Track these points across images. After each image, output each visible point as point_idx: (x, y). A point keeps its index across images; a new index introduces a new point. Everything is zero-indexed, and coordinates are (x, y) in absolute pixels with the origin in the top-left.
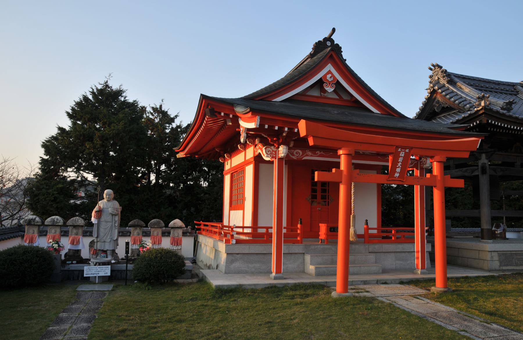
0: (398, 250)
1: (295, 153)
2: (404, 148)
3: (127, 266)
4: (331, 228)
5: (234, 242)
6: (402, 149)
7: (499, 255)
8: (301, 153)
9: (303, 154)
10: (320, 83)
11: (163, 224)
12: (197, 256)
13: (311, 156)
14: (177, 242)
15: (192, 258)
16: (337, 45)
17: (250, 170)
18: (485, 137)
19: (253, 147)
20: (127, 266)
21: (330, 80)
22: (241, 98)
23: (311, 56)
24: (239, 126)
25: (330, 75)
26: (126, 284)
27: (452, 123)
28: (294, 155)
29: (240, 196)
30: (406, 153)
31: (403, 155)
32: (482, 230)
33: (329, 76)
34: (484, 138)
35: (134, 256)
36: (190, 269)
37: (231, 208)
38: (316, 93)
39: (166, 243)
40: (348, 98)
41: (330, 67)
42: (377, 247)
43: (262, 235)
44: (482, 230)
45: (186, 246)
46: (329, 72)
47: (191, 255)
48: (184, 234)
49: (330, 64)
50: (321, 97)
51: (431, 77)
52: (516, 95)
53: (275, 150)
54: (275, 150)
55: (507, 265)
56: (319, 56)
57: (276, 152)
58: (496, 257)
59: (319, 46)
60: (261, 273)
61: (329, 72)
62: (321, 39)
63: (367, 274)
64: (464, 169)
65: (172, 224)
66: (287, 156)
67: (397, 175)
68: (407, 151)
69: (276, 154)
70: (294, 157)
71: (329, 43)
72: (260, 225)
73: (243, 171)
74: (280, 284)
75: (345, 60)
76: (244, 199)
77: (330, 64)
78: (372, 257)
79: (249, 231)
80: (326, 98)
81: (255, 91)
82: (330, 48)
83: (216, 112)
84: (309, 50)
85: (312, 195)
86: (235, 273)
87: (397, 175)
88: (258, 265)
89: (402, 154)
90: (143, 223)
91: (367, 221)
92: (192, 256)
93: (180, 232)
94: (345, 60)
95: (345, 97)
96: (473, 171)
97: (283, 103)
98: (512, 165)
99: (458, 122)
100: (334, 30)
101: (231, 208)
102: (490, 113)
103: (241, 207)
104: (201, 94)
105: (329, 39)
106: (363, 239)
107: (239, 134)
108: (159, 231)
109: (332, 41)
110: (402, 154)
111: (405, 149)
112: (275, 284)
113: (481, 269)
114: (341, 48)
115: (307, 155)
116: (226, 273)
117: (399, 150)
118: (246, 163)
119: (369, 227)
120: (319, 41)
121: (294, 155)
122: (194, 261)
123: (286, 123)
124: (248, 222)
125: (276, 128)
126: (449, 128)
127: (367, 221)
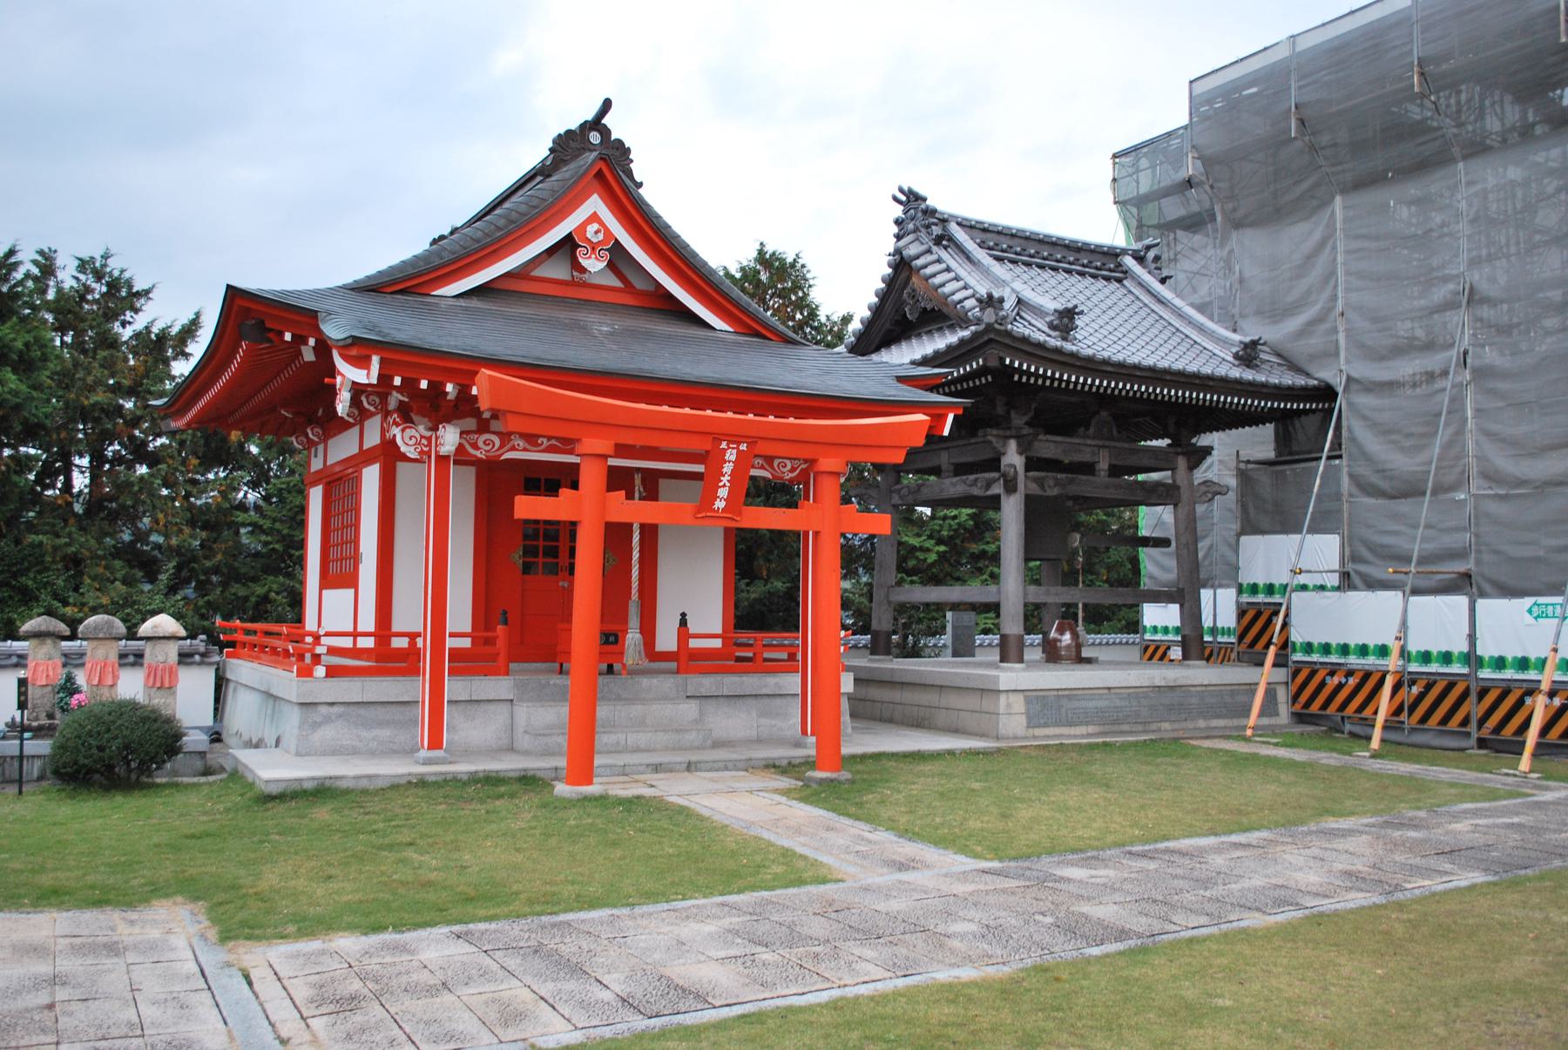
0: (765, 691)
1: (480, 444)
2: (735, 439)
3: (22, 745)
4: (616, 642)
5: (320, 671)
6: (729, 442)
7: (1028, 701)
8: (498, 444)
9: (501, 446)
10: (568, 245)
11: (120, 627)
12: (226, 721)
13: (525, 450)
14: (163, 682)
15: (209, 728)
16: (620, 142)
17: (371, 477)
18: (965, 409)
19: (378, 418)
20: (22, 745)
21: (595, 240)
22: (344, 287)
23: (541, 172)
24: (332, 371)
25: (595, 226)
26: (20, 792)
27: (913, 363)
28: (477, 448)
29: (348, 550)
30: (739, 453)
31: (733, 458)
32: (1004, 638)
33: (593, 227)
34: (960, 412)
35: (37, 719)
36: (201, 749)
37: (327, 581)
38: (557, 270)
39: (131, 686)
40: (651, 288)
41: (594, 203)
42: (707, 683)
43: (400, 655)
44: (1004, 638)
45: (190, 699)
46: (594, 218)
47: (208, 720)
48: (185, 658)
49: (595, 197)
50: (572, 283)
51: (898, 222)
52: (1119, 281)
53: (427, 434)
54: (427, 434)
55: (1046, 725)
56: (567, 175)
57: (429, 439)
58: (1018, 704)
59: (567, 145)
60: (395, 752)
61: (594, 218)
62: (574, 125)
63: (674, 749)
64: (972, 477)
65: (146, 628)
66: (460, 449)
67: (720, 504)
68: (743, 447)
69: (429, 445)
70: (478, 453)
71: (595, 138)
72: (396, 628)
73: (357, 481)
74: (436, 774)
75: (640, 185)
76: (356, 558)
77: (595, 197)
78: (690, 709)
79: (367, 643)
80: (585, 285)
81: (383, 265)
82: (595, 154)
83: (270, 330)
84: (537, 152)
85: (525, 547)
86: (324, 754)
87: (720, 504)
88: (385, 733)
89: (731, 455)
90: (63, 628)
91: (683, 615)
92: (209, 721)
93: (171, 651)
94: (640, 185)
95: (639, 284)
96: (988, 485)
97: (462, 302)
98: (1088, 468)
99: (925, 361)
100: (607, 105)
101: (327, 581)
102: (1007, 341)
103: (349, 580)
104: (229, 286)
105: (596, 124)
106: (673, 665)
107: (332, 392)
108: (110, 652)
109: (605, 132)
110: (731, 455)
111: (739, 443)
112: (423, 775)
113: (955, 731)
114: (628, 150)
115: (513, 449)
116: (298, 754)
117: (724, 445)
118: (365, 457)
119: (691, 631)
120: (569, 132)
121: (477, 448)
122: (216, 737)
123: (452, 374)
124: (368, 622)
125: (424, 384)
126: (900, 379)
127: (683, 615)
